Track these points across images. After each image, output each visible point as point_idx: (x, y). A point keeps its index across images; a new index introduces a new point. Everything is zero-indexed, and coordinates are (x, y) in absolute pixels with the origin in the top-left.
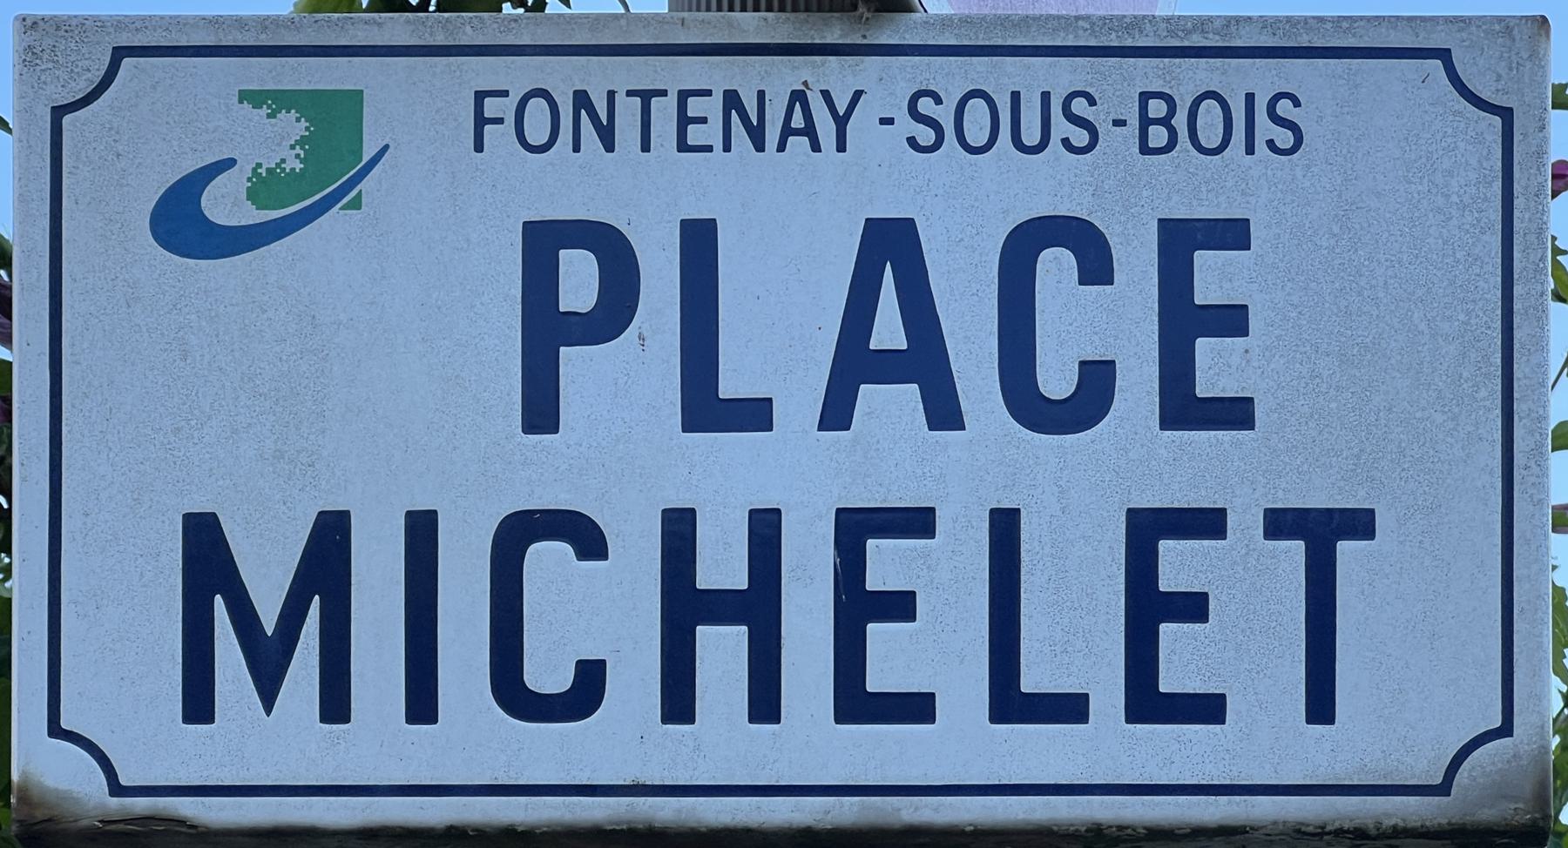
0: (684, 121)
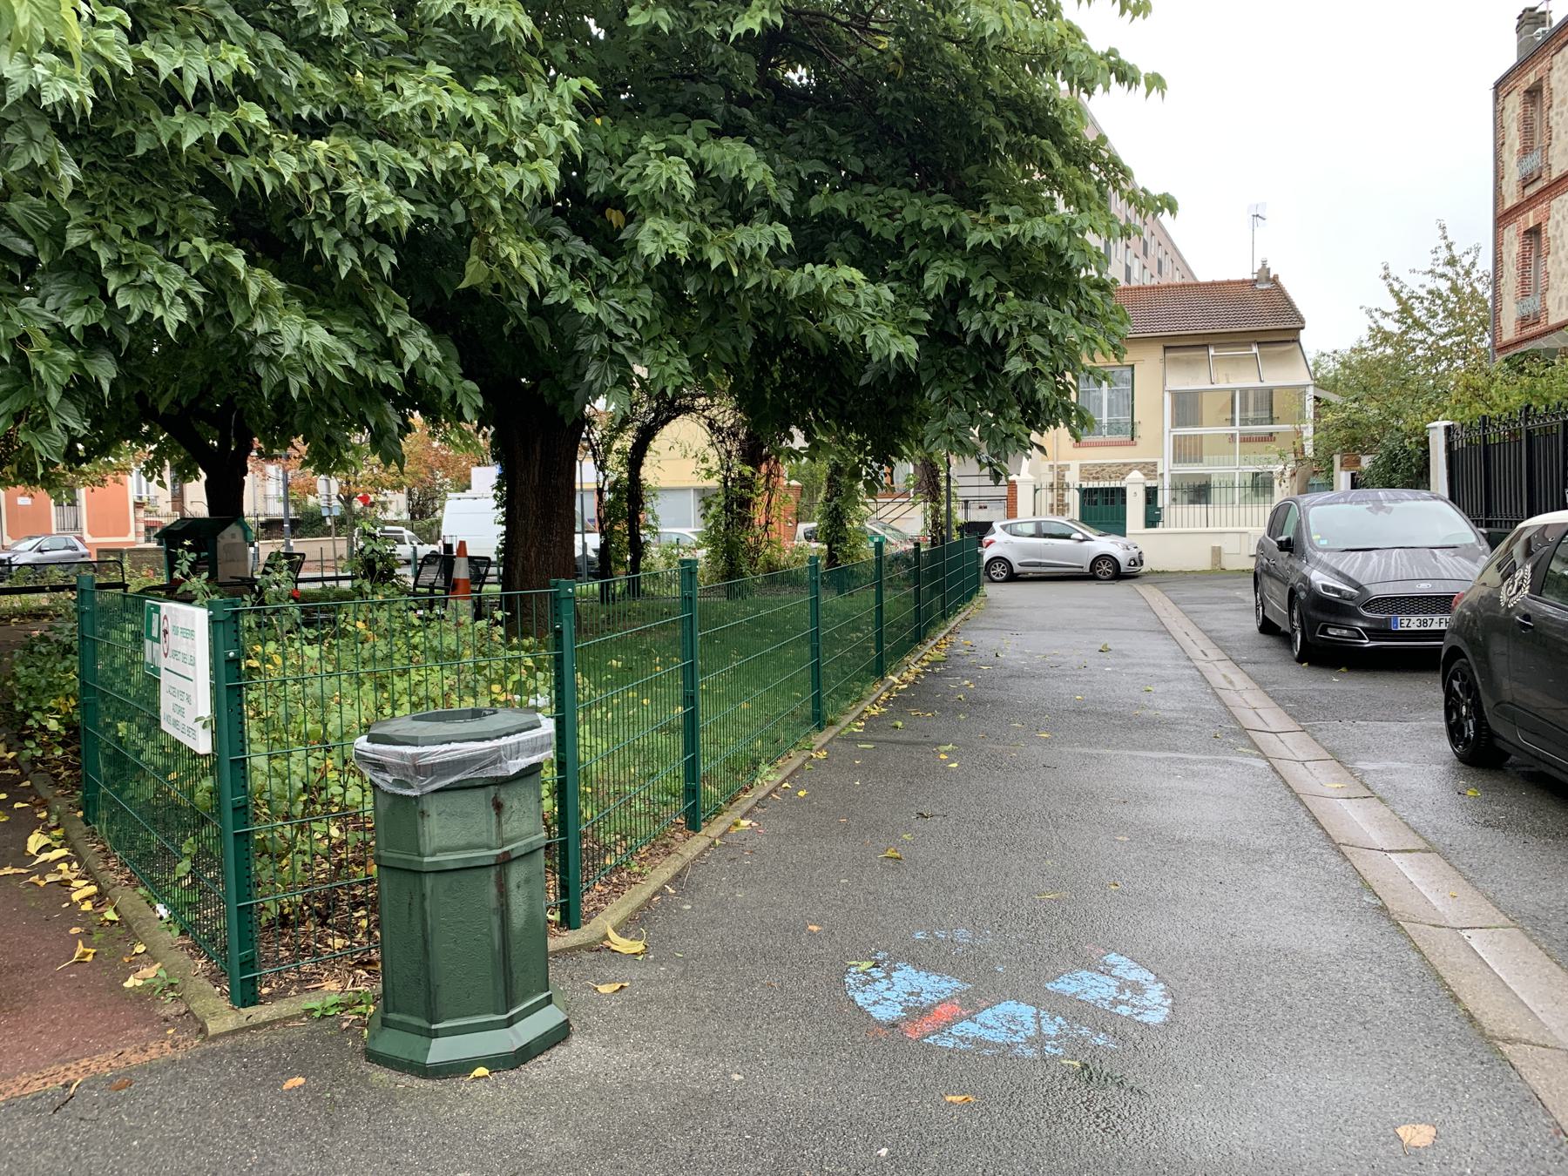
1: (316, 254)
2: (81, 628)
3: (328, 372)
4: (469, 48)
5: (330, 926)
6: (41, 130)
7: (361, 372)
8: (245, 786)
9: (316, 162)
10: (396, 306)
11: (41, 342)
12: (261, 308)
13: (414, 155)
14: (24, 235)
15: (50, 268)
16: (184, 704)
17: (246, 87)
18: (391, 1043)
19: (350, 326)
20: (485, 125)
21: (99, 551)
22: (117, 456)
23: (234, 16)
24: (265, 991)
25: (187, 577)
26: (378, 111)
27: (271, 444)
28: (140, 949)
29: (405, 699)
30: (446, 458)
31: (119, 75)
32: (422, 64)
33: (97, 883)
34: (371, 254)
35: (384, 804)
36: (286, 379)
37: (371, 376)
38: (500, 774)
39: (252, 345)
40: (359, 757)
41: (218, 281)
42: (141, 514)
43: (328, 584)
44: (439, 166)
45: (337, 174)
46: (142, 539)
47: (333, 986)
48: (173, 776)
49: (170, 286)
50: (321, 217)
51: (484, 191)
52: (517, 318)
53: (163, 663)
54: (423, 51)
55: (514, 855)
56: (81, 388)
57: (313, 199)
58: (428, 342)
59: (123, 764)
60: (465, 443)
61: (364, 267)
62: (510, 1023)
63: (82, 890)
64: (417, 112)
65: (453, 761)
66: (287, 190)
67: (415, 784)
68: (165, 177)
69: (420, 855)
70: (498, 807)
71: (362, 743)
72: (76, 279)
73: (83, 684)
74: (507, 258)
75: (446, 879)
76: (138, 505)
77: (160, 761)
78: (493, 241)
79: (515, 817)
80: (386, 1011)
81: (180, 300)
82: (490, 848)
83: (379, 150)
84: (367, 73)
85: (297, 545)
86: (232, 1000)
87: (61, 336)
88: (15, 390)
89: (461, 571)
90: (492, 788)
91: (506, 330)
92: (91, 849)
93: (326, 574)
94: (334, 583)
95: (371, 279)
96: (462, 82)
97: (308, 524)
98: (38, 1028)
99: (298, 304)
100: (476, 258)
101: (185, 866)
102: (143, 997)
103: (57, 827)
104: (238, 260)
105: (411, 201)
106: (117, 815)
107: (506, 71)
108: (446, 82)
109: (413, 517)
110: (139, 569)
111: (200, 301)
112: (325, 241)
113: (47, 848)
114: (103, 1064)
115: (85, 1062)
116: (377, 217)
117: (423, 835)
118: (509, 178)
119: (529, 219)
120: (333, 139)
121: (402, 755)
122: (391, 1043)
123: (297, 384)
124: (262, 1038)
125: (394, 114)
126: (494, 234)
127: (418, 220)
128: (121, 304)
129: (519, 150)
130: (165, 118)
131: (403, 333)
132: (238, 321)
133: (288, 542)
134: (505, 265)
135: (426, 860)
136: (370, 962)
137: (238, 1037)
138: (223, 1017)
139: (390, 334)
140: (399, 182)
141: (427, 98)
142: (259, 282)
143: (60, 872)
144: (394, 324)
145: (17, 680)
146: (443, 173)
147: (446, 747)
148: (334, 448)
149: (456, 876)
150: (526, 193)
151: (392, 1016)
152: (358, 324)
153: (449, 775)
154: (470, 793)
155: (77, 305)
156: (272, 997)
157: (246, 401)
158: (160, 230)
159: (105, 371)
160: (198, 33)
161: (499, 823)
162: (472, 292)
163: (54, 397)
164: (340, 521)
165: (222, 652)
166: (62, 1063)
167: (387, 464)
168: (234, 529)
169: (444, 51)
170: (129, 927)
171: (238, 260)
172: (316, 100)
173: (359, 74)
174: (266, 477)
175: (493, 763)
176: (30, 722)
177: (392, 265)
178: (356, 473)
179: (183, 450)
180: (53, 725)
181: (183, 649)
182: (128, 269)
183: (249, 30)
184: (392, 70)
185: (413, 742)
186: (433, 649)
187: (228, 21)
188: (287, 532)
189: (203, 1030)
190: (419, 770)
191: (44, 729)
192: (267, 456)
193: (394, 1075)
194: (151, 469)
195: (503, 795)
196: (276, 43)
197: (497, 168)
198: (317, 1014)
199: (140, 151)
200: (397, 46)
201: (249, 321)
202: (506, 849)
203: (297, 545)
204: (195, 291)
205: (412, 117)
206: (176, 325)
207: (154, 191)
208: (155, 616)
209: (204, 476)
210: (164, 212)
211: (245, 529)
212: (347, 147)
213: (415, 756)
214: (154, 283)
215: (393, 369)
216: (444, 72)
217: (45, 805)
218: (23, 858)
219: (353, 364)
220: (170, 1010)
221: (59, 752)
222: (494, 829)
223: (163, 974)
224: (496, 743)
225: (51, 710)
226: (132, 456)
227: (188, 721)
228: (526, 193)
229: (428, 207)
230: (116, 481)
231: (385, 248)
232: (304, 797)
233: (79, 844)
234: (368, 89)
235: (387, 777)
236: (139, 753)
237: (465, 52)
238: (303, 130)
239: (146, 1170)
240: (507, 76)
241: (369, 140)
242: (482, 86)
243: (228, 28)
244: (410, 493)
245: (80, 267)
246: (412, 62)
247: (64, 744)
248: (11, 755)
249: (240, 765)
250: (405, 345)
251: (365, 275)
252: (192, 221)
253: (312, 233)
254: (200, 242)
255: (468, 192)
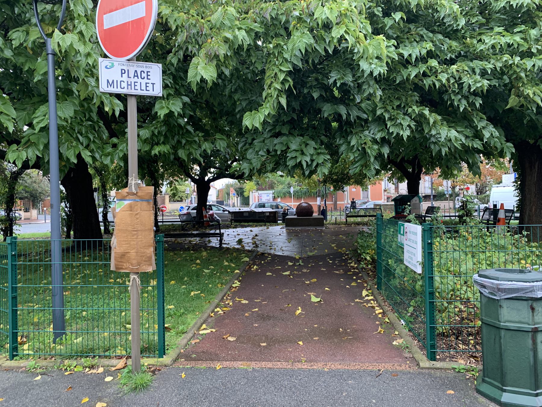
0: (135, 86)
1: (452, 105)
2: (377, 229)
3: (455, 146)
4: (510, 18)
5: (459, 340)
6: (372, 82)
7: (467, 144)
8: (433, 286)
9: (453, 73)
10: (481, 118)
11: (369, 144)
12: (434, 126)
13: (489, 63)
14: (365, 112)
15: (372, 121)
16: (413, 256)
17: (430, 54)
18: (485, 388)
19: (463, 128)
20: (518, 44)
21: (374, 205)
22: (380, 176)
23: (426, 31)
24: (438, 357)
25: (409, 214)
26: (475, 50)
27: (428, 169)
28: (397, 333)
29: (484, 262)
30: (492, 171)
31: (393, 59)
32: (492, 29)
33: (382, 309)
34: (472, 101)
35: (484, 300)
36: (441, 149)
37: (470, 145)
38: (534, 296)
39: (430, 139)
40: (475, 281)
41: (420, 120)
42: (386, 193)
43: (452, 218)
44: (499, 65)
45: (460, 75)
46: (386, 201)
47: (462, 362)
48: (405, 279)
49: (405, 124)
50: (454, 92)
51: (518, 71)
52: (530, 116)
53: (405, 242)
54: (492, 24)
55: (539, 329)
56: (379, 156)
57: (451, 86)
58: (494, 130)
59: (389, 273)
60: (501, 166)
61: (469, 107)
62: (537, 395)
63: (378, 311)
64: (490, 47)
65: (513, 289)
66: (443, 85)
67: (497, 294)
68: (404, 88)
69: (499, 321)
70: (533, 309)
71: (476, 276)
72: (379, 123)
73: (378, 246)
74: (528, 94)
75: (510, 333)
76: (385, 191)
77: (401, 274)
78: (521, 89)
79: (540, 314)
80: (484, 376)
81: (408, 128)
82: (529, 324)
83: (477, 64)
84: (471, 37)
85: (436, 204)
86: (427, 357)
87: (374, 141)
88: (362, 158)
89: (501, 215)
90: (530, 301)
91: (525, 122)
92: (380, 298)
93: (451, 214)
94: (454, 218)
95: (472, 110)
96: (508, 31)
97: (440, 196)
98: (370, 350)
99: (445, 123)
100: (514, 96)
101: (411, 309)
102: (398, 348)
103: (370, 289)
104: (426, 112)
105: (488, 80)
106: (388, 288)
107: (526, 22)
108: (501, 33)
109: (477, 194)
110: (386, 211)
111: (413, 127)
112: (455, 100)
113: (367, 295)
114: (389, 366)
115: (383, 364)
116: (475, 88)
117: (501, 314)
118: (528, 63)
119: (537, 77)
120: (459, 64)
121: (493, 283)
122: (485, 388)
123: (444, 150)
124: (438, 373)
125: (482, 50)
126: (522, 86)
127: (490, 86)
128: (391, 131)
129: (534, 50)
130: (405, 70)
131: (484, 128)
132: (426, 131)
133: (432, 203)
134: (527, 97)
135: (502, 324)
136: (475, 357)
137: (430, 370)
138: (425, 363)
139: (479, 129)
140: (484, 74)
141: (495, 41)
142: (433, 117)
143: (372, 303)
144: (480, 125)
145: (358, 243)
146: (500, 67)
147: (510, 283)
148: (450, 170)
149: (514, 332)
150: (536, 68)
151: (487, 379)
152: (466, 127)
153: (512, 294)
154: (521, 302)
155: (379, 131)
156: (440, 360)
157: (422, 156)
158: (402, 106)
159: (386, 151)
160: (415, 40)
161: (533, 315)
162: (511, 109)
163: (372, 159)
164: (451, 195)
165: (426, 240)
166: (377, 363)
167: (475, 176)
168: (416, 198)
169: (500, 22)
170: (393, 325)
171: (426, 112)
172: (452, 51)
173: (468, 39)
174: (425, 181)
175: (531, 291)
176: (362, 256)
177: (480, 104)
178: (457, 178)
179: (400, 172)
180: (368, 258)
181: (412, 239)
182: (393, 120)
183: (431, 35)
184: (480, 34)
185: (497, 279)
186: (495, 245)
187: (424, 34)
188: (432, 199)
189: (418, 365)
190: (499, 290)
191: (366, 259)
192: (426, 173)
193: (488, 401)
194: (390, 179)
195: (535, 305)
196: (440, 37)
197: (524, 61)
198: (457, 370)
199: (398, 82)
200: (481, 25)
201: (430, 131)
202: (536, 326)
203: (436, 204)
204: (413, 124)
205: (488, 49)
206: (406, 137)
207: (401, 93)
208: (402, 227)
209: (406, 181)
210: (404, 99)
211: (419, 197)
212: (464, 65)
213: (497, 284)
214: (401, 123)
215: (479, 142)
216: (501, 29)
217: (366, 282)
218: (361, 298)
219: (464, 142)
220: (407, 355)
221: (370, 266)
222: (531, 317)
223: (404, 343)
224: (532, 284)
225: (368, 253)
226: (385, 176)
227: (415, 262)
228: (536, 68)
229: (494, 81)
230: (379, 183)
231: (478, 98)
232: (451, 293)
233: (376, 296)
234: (471, 43)
235: (486, 290)
236: (395, 270)
237: (508, 20)
238: (447, 63)
239: (404, 405)
240: (526, 24)
241: (472, 61)
242: (516, 30)
243: (424, 36)
244: (476, 185)
245: (381, 121)
246: (488, 29)
247: (371, 264)
248: (356, 265)
249: (431, 279)
250: (484, 132)
251: (470, 109)
252: (412, 101)
253: (450, 97)
254: (414, 107)
255: (511, 72)
